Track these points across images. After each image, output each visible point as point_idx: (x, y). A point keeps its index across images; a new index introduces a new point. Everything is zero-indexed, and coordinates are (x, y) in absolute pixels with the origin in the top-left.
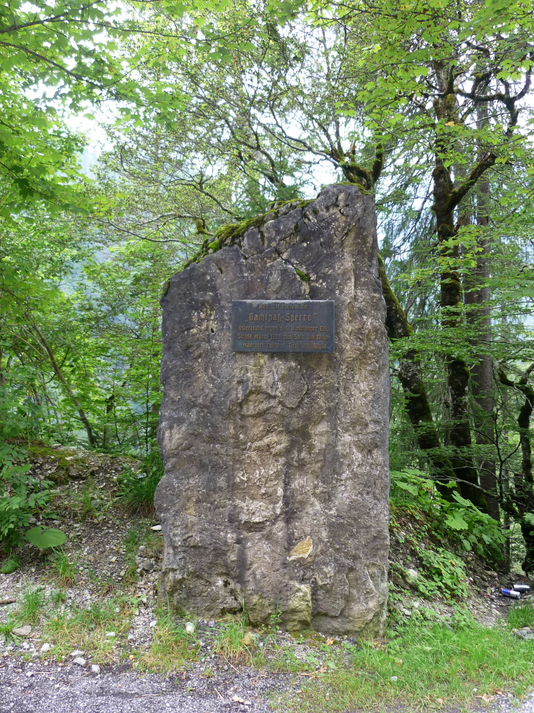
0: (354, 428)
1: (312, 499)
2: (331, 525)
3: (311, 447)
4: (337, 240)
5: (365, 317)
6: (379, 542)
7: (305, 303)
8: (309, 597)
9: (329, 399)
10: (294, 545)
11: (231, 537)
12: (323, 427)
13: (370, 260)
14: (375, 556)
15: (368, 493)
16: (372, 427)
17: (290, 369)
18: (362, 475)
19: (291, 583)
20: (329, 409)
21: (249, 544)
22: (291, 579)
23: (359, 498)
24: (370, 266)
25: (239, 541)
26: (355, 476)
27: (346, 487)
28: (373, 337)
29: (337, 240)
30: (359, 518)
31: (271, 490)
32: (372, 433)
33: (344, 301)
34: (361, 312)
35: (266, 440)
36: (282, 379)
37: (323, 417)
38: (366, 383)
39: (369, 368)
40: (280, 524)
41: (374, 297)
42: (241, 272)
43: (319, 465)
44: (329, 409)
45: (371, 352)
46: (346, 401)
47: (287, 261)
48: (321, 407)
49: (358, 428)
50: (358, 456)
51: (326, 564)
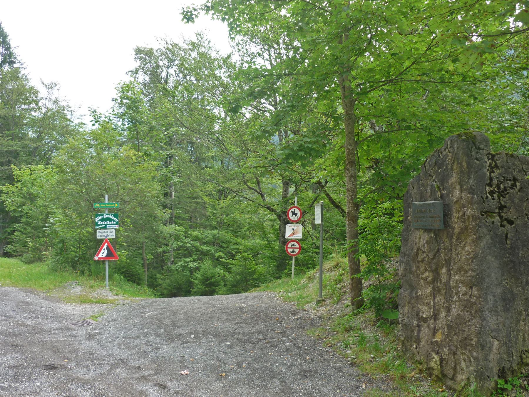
0: (460, 272)
1: (442, 309)
2: (448, 325)
3: (441, 281)
4: (449, 167)
5: (465, 209)
6: (468, 341)
7: (421, 205)
8: (438, 363)
9: (446, 255)
10: (436, 333)
11: (415, 323)
12: (444, 270)
13: (469, 175)
14: (466, 349)
15: (467, 312)
16: (470, 273)
17: (431, 237)
18: (464, 300)
19: (432, 353)
20: (446, 260)
21: (422, 329)
22: (432, 351)
23: (462, 313)
24: (469, 179)
25: (418, 326)
26: (460, 300)
27: (456, 305)
28: (471, 220)
29: (449, 167)
30: (460, 324)
31: (429, 301)
32: (470, 276)
33: (453, 200)
34: (464, 206)
35: (205, 248)
36: (427, 242)
37: (443, 264)
38: (469, 247)
39: (471, 238)
40: (432, 321)
41: (468, 197)
42: (420, 188)
43: (444, 291)
44: (446, 260)
45: (471, 229)
46: (454, 256)
47: (434, 181)
48: (442, 259)
49: (462, 273)
50: (463, 289)
51: (445, 347)
